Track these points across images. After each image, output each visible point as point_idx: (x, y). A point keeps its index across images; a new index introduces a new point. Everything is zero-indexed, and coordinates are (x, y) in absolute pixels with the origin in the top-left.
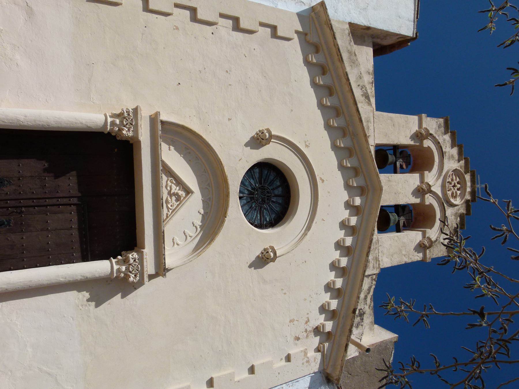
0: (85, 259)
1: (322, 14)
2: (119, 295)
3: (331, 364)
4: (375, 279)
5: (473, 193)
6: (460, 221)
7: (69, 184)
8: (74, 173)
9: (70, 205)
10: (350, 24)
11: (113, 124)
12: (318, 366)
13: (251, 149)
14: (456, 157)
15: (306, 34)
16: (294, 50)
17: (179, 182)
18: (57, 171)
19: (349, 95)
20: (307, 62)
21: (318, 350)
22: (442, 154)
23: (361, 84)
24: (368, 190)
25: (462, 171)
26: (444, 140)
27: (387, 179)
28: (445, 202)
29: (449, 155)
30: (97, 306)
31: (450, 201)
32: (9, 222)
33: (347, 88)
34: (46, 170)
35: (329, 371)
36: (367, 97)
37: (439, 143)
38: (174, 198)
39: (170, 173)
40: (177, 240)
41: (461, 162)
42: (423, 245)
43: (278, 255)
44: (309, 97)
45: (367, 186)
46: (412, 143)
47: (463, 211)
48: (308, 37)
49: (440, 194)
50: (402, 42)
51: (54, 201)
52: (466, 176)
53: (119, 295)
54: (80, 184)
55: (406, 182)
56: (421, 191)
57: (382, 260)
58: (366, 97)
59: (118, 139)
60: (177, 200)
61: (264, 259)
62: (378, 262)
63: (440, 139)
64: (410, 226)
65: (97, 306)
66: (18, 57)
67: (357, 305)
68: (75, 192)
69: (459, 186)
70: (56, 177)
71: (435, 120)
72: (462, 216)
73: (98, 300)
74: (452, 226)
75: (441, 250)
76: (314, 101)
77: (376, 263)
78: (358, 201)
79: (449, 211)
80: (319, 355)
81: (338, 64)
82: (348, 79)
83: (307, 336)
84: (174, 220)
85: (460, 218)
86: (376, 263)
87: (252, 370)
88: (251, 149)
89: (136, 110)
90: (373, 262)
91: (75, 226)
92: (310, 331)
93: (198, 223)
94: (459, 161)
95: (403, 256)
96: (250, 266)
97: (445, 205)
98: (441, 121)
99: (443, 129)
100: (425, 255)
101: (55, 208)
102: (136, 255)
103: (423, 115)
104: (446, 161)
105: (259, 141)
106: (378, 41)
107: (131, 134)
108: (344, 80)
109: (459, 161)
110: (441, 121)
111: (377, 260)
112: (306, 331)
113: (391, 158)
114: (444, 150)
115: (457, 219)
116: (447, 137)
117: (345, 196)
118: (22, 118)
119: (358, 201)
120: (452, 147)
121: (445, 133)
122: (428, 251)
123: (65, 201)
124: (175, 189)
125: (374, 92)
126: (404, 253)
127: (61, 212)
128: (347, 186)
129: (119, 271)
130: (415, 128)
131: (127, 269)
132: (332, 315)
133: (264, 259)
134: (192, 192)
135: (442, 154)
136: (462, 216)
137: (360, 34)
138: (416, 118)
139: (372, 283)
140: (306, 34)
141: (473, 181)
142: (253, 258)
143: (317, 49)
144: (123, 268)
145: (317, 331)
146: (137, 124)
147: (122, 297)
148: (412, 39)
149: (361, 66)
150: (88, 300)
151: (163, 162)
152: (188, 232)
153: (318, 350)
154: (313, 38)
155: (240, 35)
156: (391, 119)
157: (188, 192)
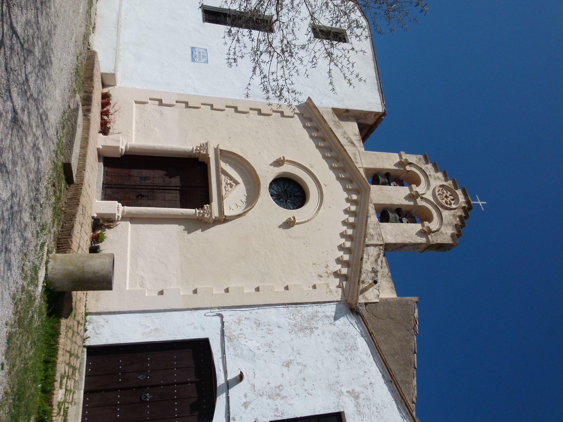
0: (182, 207)
1: (311, 104)
2: (200, 230)
3: (350, 295)
5: (468, 202)
7: (176, 181)
8: (178, 177)
9: (176, 190)
10: (333, 109)
11: (196, 150)
12: (340, 297)
15: (303, 114)
16: (297, 122)
17: (231, 178)
18: (171, 175)
19: (335, 139)
20: (305, 127)
21: (339, 287)
22: (424, 172)
25: (452, 187)
26: (427, 168)
30: (188, 233)
32: (148, 196)
33: (333, 136)
34: (165, 175)
35: (349, 300)
36: (352, 143)
38: (229, 186)
39: (226, 174)
40: (232, 207)
43: (297, 221)
44: (311, 144)
47: (460, 213)
48: (304, 115)
49: (432, 200)
50: (379, 117)
51: (169, 188)
52: (457, 191)
53: (200, 230)
54: (181, 181)
56: (413, 197)
59: (200, 160)
60: (231, 187)
61: (289, 224)
63: (424, 167)
65: (188, 233)
66: (156, 129)
68: (178, 184)
70: (170, 177)
73: (189, 230)
76: (313, 145)
78: (354, 197)
79: (445, 213)
80: (340, 290)
81: (325, 125)
82: (332, 131)
83: (328, 276)
84: (231, 196)
87: (287, 288)
89: (207, 144)
91: (178, 199)
92: (331, 274)
93: (244, 199)
96: (280, 227)
97: (440, 208)
98: (421, 156)
101: (169, 191)
102: (202, 152)
105: (279, 163)
106: (363, 121)
107: (205, 153)
108: (330, 132)
112: (327, 273)
113: (379, 177)
114: (428, 173)
115: (456, 219)
116: (430, 166)
117: (345, 195)
118: (157, 146)
119: (354, 197)
123: (174, 188)
124: (229, 182)
127: (172, 193)
128: (346, 189)
129: (199, 213)
130: (398, 160)
131: (204, 212)
132: (346, 264)
133: (289, 224)
134: (239, 183)
135: (424, 172)
137: (344, 115)
140: (303, 114)
142: (281, 223)
143: (311, 120)
144: (202, 211)
145: (336, 274)
146: (207, 149)
147: (202, 231)
148: (384, 114)
149: (350, 131)
150: (184, 230)
151: (222, 168)
152: (238, 204)
153: (339, 287)
154: (307, 115)
155: (263, 117)
156: (375, 155)
157: (237, 183)
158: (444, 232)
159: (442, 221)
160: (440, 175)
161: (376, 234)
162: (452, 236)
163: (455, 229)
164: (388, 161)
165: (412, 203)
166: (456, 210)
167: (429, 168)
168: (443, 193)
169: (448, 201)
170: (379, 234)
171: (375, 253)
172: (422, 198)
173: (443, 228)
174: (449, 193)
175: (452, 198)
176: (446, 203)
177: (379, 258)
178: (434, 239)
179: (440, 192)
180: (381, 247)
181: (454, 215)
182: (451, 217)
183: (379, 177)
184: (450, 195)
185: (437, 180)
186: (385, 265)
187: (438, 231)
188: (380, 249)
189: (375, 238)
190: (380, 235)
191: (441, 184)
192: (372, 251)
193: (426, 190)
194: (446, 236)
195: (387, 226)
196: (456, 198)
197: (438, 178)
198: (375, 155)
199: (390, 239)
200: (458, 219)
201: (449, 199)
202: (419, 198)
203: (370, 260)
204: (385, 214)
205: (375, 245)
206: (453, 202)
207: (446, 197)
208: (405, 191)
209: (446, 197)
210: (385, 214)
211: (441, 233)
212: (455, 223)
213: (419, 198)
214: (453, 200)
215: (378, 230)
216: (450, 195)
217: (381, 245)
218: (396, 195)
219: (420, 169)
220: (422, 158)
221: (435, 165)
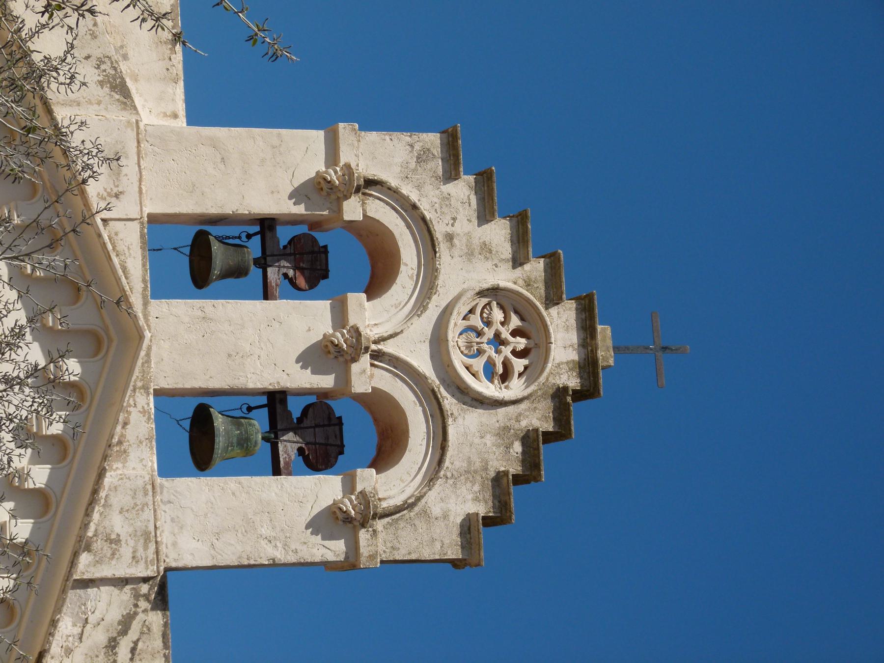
4: (146, 597)
5: (588, 366)
6: (524, 453)
13: (313, 373)
14: (506, 250)
23: (97, 53)
24: (110, 340)
26: (446, 199)
27: (200, 313)
28: (446, 390)
29: (469, 245)
31: (468, 387)
37: (415, 207)
41: (527, 267)
42: (340, 516)
45: (106, 329)
46: (300, 209)
47: (539, 418)
55: (276, 325)
57: (175, 544)
58: (113, 88)
62: (152, 547)
63: (427, 197)
64: (319, 459)
67: (50, 643)
69: (521, 343)
71: (406, 138)
72: (531, 441)
74: (486, 469)
75: (433, 540)
77: (146, 548)
78: (73, 368)
79: (465, 424)
85: (523, 445)
86: (146, 548)
88: (313, 373)
90: (132, 543)
94: (517, 262)
95: (263, 543)
99: (438, 166)
100: (353, 547)
103: (341, 125)
104: (447, 261)
109: (517, 262)
110: (433, 140)
111: (147, 540)
114: (440, 229)
115: (508, 447)
119: (73, 368)
120: (485, 216)
121: (451, 174)
122: (363, 535)
125: (180, 67)
126: (265, 531)
136: (531, 441)
138: (318, 136)
139: (136, 606)
141: (587, 328)
156: (214, 144)
158: (436, 511)
159: (440, 462)
160: (498, 232)
161: (133, 535)
162: (468, 527)
163: (488, 495)
164: (262, 171)
165: (326, 382)
166: (523, 406)
167: (452, 203)
168: (488, 323)
169: (499, 361)
170: (146, 536)
171: (115, 615)
172: (377, 356)
173: (429, 501)
174: (515, 322)
175: (521, 343)
176: (489, 367)
177: (124, 632)
178: (378, 544)
179: (476, 321)
180: (144, 588)
181: (503, 432)
182: (489, 440)
183: (209, 255)
184: (515, 333)
185: (478, 257)
186: (158, 643)
187: (407, 506)
188: (137, 596)
189: (126, 551)
190: (150, 537)
191: (490, 281)
192: (102, 606)
193: (409, 318)
194: (438, 529)
195: (197, 491)
196: (536, 348)
197: (486, 250)
198: (214, 144)
199: (189, 550)
200: (518, 447)
201: (507, 351)
202: (366, 359)
203: (87, 642)
204: (200, 435)
205: (121, 582)
206: (519, 364)
207: (498, 341)
208: (306, 319)
209: (498, 341)
210: (200, 435)
211: (425, 513)
212: (498, 464)
213: (366, 359)
214: (517, 354)
215: (148, 514)
216: (515, 333)
217: (145, 580)
218: (262, 341)
219: (410, 210)
220: (437, 151)
221: (484, 183)
